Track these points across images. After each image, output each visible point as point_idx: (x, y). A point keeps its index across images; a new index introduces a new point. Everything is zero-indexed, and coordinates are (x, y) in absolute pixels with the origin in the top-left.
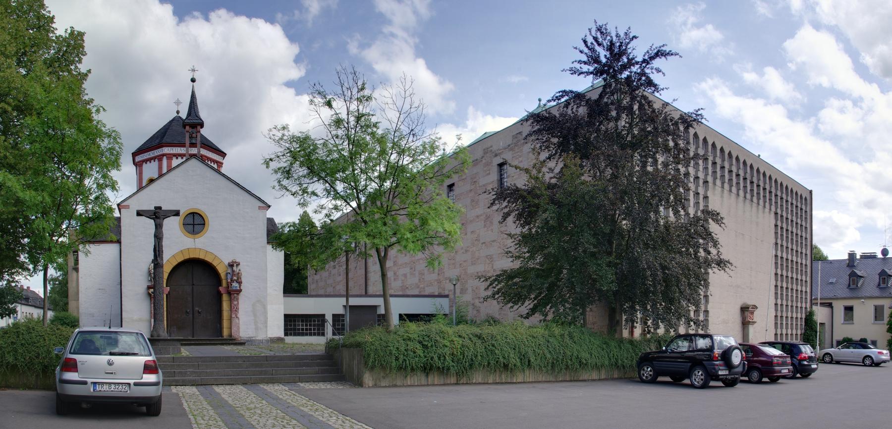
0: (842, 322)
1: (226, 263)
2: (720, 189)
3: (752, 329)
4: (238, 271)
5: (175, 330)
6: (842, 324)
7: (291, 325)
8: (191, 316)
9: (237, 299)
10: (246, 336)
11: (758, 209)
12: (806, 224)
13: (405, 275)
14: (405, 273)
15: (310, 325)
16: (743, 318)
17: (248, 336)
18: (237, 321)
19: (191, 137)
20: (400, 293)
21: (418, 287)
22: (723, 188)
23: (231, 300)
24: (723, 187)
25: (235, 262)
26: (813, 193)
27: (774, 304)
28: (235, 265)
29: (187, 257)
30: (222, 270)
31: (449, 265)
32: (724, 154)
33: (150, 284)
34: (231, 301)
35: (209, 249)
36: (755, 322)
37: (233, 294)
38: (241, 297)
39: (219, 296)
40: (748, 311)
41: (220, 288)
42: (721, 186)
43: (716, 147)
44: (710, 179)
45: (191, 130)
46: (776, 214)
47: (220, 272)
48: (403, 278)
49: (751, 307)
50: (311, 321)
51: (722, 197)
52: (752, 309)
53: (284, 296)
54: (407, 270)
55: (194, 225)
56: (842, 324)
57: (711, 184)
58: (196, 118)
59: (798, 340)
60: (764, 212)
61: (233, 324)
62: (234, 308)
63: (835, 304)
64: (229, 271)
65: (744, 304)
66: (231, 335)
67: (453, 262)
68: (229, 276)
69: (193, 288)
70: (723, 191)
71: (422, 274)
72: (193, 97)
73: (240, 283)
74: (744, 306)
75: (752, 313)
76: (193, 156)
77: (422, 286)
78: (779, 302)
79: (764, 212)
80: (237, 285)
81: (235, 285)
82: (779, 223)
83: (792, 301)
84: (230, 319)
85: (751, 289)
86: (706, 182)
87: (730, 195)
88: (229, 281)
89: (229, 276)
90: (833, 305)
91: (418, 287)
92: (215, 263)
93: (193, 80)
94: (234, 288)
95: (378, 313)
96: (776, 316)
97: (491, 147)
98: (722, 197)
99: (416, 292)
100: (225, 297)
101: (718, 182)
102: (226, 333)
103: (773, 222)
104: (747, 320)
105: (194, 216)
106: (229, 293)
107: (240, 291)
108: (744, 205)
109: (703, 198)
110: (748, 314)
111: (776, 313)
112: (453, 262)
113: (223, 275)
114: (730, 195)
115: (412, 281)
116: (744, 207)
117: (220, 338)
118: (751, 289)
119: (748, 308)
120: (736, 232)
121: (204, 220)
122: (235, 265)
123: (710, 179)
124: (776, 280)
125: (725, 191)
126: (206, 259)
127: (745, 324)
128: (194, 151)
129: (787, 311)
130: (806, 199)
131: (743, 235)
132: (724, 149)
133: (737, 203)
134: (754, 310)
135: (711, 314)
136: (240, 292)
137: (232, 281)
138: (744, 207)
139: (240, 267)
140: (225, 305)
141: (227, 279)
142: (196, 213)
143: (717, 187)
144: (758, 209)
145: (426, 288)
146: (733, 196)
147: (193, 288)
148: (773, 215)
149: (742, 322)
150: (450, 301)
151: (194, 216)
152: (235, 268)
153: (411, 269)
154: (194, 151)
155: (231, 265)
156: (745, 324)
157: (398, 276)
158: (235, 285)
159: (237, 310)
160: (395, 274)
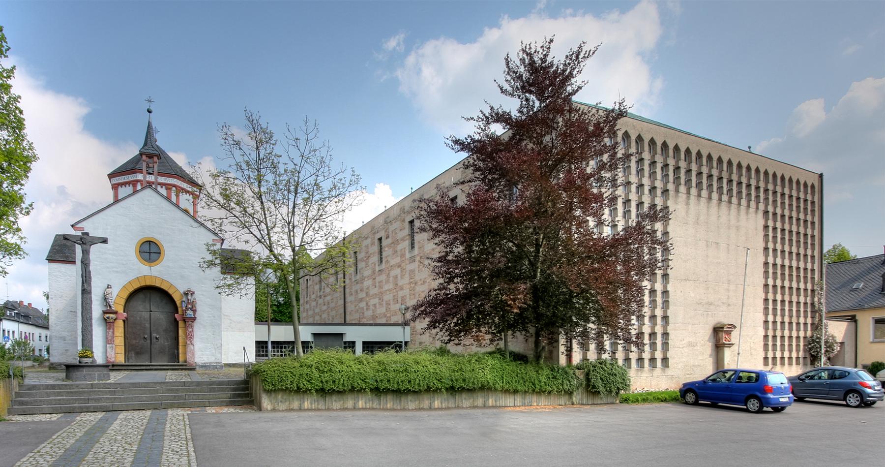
0: (871, 340)
1: (182, 292)
2: (685, 196)
3: (728, 354)
4: (192, 299)
5: (133, 355)
6: (872, 343)
7: (263, 351)
8: (149, 341)
9: (192, 327)
10: (201, 362)
11: (739, 210)
12: (813, 218)
13: (375, 305)
14: (375, 303)
15: (278, 351)
16: (716, 340)
17: (203, 362)
18: (192, 347)
19: (148, 167)
20: (371, 322)
21: (386, 316)
22: (689, 194)
23: (186, 327)
24: (688, 193)
25: (190, 291)
26: (825, 178)
27: (762, 322)
28: (190, 293)
29: (143, 284)
30: (176, 298)
31: (410, 295)
32: (691, 156)
33: (105, 309)
34: (186, 327)
35: (165, 277)
36: (733, 344)
37: (189, 321)
38: (196, 325)
39: (176, 322)
40: (722, 331)
41: (176, 315)
42: (686, 192)
43: (680, 150)
44: (671, 187)
45: (148, 160)
46: (766, 212)
47: (176, 300)
48: (373, 308)
49: (726, 327)
50: (282, 348)
51: (687, 204)
52: (728, 329)
53: (256, 324)
54: (376, 301)
55: (150, 253)
56: (872, 343)
57: (672, 193)
58: (152, 149)
59: (768, 365)
60: (747, 213)
61: (188, 350)
62: (189, 335)
63: (860, 316)
64: (184, 299)
65: (717, 324)
66: (186, 361)
67: (412, 292)
68: (184, 304)
69: (150, 314)
70: (688, 198)
71: (388, 304)
72: (149, 126)
73: (194, 311)
74: (719, 325)
75: (729, 333)
76: (150, 185)
77: (388, 315)
78: (770, 318)
79: (747, 213)
80: (192, 313)
81: (190, 312)
82: (770, 223)
83: (791, 317)
84: (185, 345)
85: (729, 305)
86: (665, 192)
87: (699, 200)
88: (184, 309)
89: (184, 304)
90: (857, 318)
91: (386, 316)
92: (171, 292)
93: (149, 111)
94: (189, 316)
95: (344, 340)
96: (766, 337)
97: (444, 183)
98: (687, 204)
99: (384, 321)
100: (181, 324)
101: (683, 189)
102: (181, 359)
103: (761, 222)
104: (721, 342)
105: (150, 244)
106: (184, 321)
107: (194, 319)
108: (719, 209)
109: (697, 175)
110: (722, 336)
111: (766, 332)
112: (412, 292)
113: (178, 303)
114: (699, 200)
115: (381, 310)
116: (718, 212)
117: (176, 364)
118: (729, 305)
119: (723, 328)
120: (707, 242)
121: (160, 249)
122: (190, 293)
123: (671, 187)
124: (767, 293)
125: (692, 197)
126: (162, 287)
127: (719, 347)
128: (151, 178)
129: (783, 329)
130: (813, 186)
131: (717, 243)
132: (691, 149)
133: (708, 208)
134: (730, 329)
135: (671, 337)
136: (195, 320)
137: (187, 309)
138: (718, 212)
139: (194, 296)
140: (181, 332)
141: (182, 307)
142: (152, 242)
143: (680, 195)
144: (739, 210)
145: (392, 317)
146: (703, 201)
147: (150, 314)
148: (760, 214)
149: (716, 345)
150: (411, 329)
151: (150, 244)
152: (189, 297)
153: (380, 299)
154: (151, 178)
155: (186, 294)
156: (719, 347)
157: (369, 306)
158: (190, 312)
159: (192, 337)
160: (367, 304)
